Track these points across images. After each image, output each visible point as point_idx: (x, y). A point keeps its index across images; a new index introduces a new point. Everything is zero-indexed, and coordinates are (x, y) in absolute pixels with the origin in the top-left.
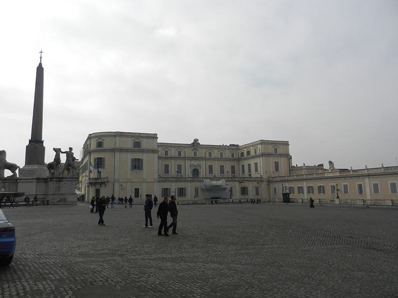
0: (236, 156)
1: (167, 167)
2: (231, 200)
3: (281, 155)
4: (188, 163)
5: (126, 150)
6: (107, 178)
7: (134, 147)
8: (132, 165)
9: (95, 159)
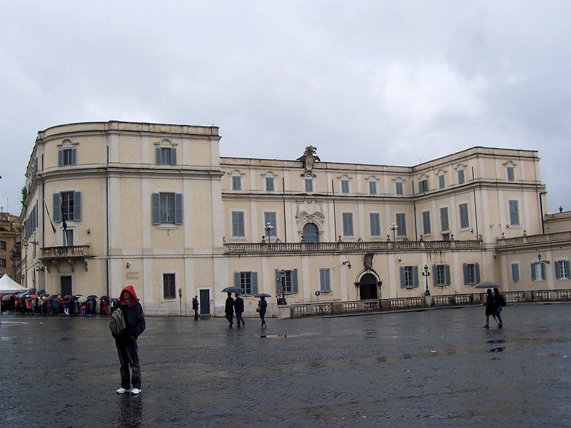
0: (406, 192)
1: (238, 219)
3: (522, 186)
4: (291, 208)
5: (139, 172)
7: (158, 162)
9: (56, 196)
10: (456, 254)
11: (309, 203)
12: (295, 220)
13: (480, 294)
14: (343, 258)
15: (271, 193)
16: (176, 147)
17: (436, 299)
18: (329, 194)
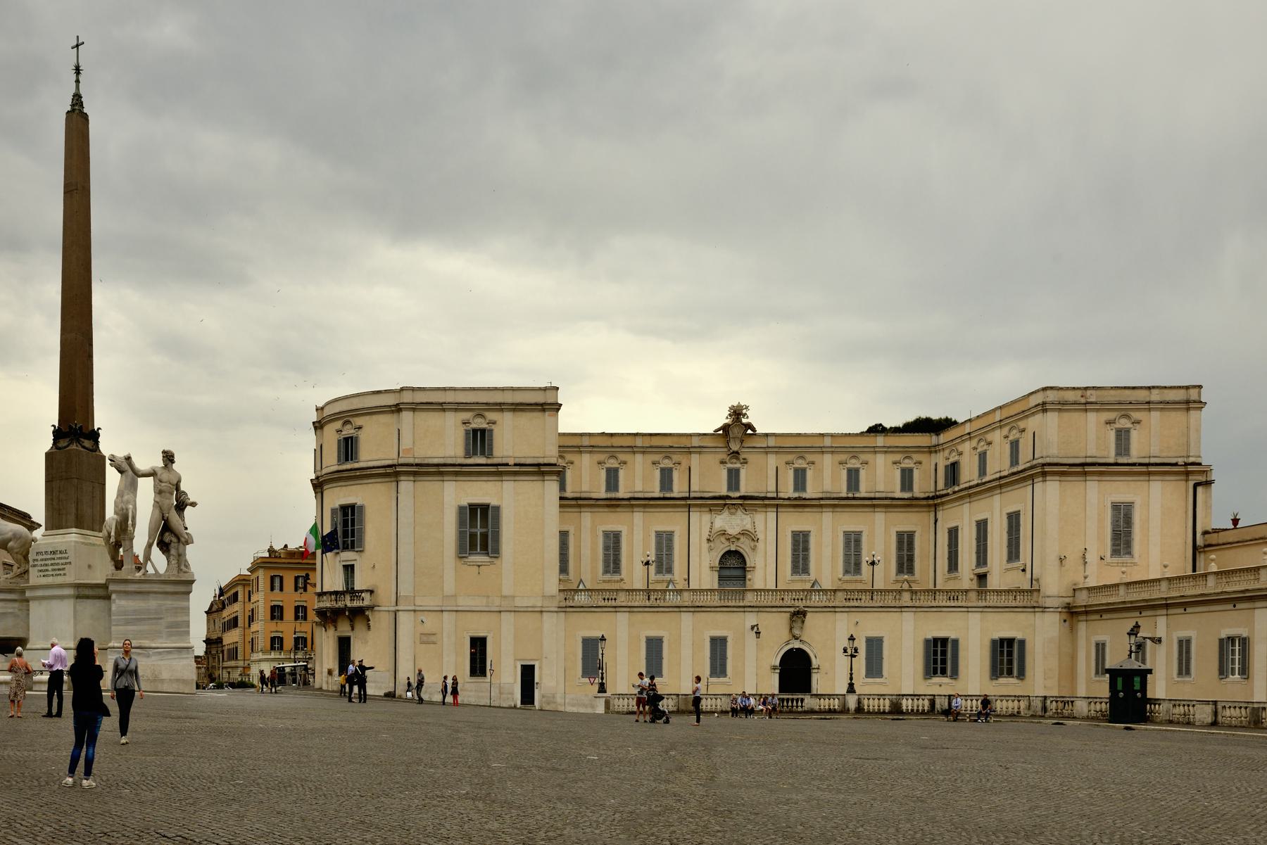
0: (922, 486)
2: (852, 702)
4: (702, 522)
6: (371, 592)
7: (468, 454)
8: (461, 535)
9: (333, 511)
10: (975, 618)
11: (732, 514)
12: (705, 545)
13: (950, 696)
14: (751, 619)
15: (668, 495)
16: (493, 427)
17: (866, 702)
18: (769, 495)
